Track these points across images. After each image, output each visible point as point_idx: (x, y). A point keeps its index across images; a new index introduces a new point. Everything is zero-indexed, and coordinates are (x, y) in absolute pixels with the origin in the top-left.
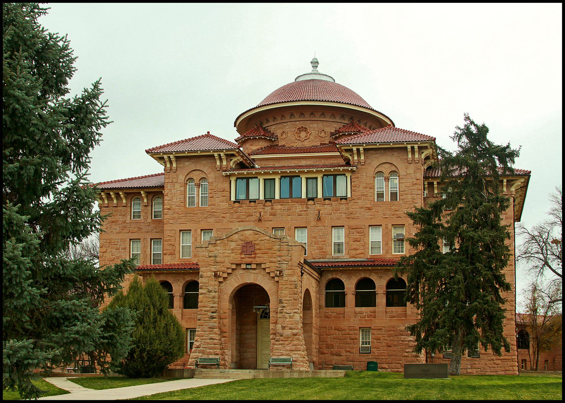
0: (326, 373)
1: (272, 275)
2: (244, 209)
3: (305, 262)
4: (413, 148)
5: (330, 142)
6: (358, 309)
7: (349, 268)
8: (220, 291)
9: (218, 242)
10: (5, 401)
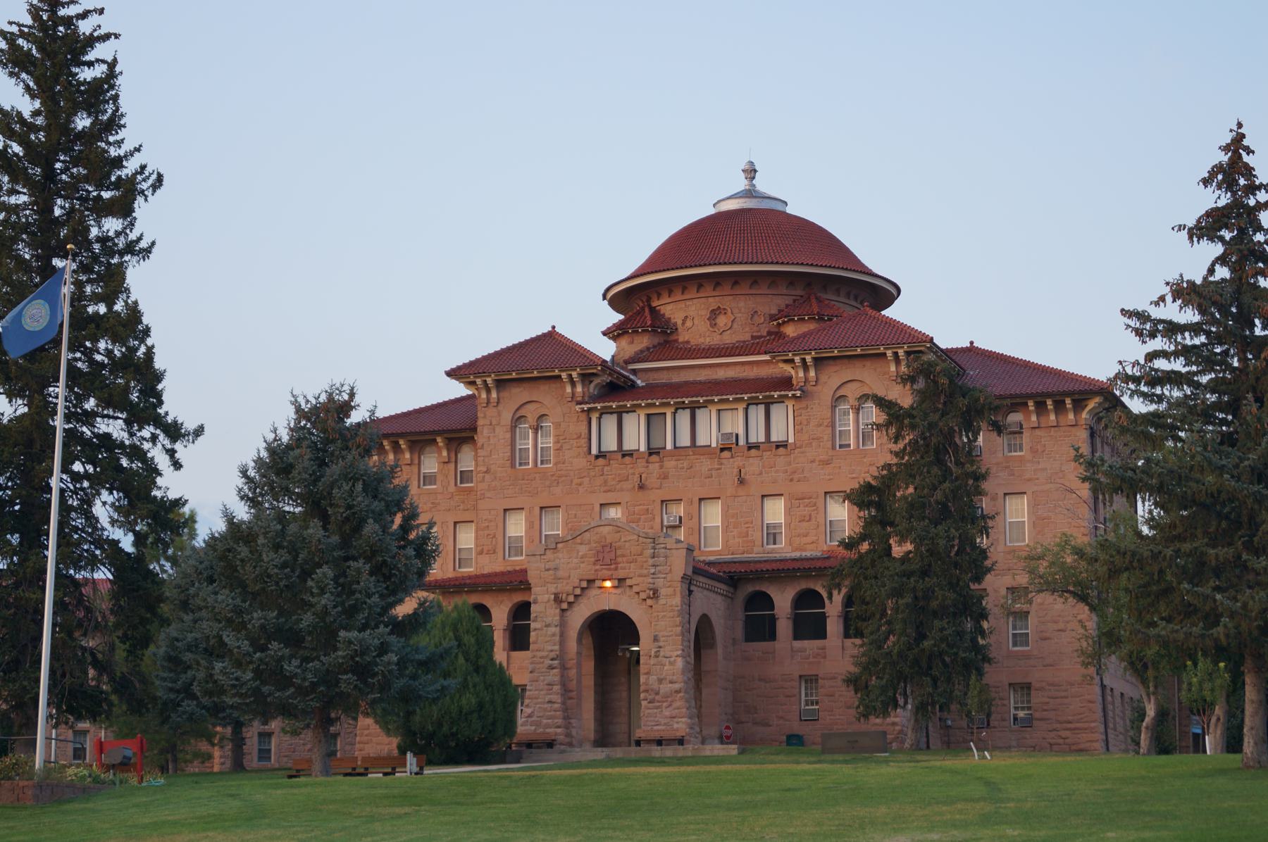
0: (712, 750)
2: (616, 468)
3: (697, 571)
5: (769, 333)
6: (797, 644)
7: (783, 571)
8: (563, 625)
9: (560, 546)
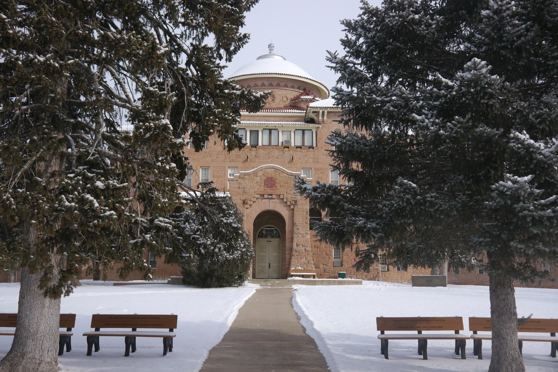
1: (288, 204)
4: (323, 112)
9: (246, 177)
10: (492, 312)
